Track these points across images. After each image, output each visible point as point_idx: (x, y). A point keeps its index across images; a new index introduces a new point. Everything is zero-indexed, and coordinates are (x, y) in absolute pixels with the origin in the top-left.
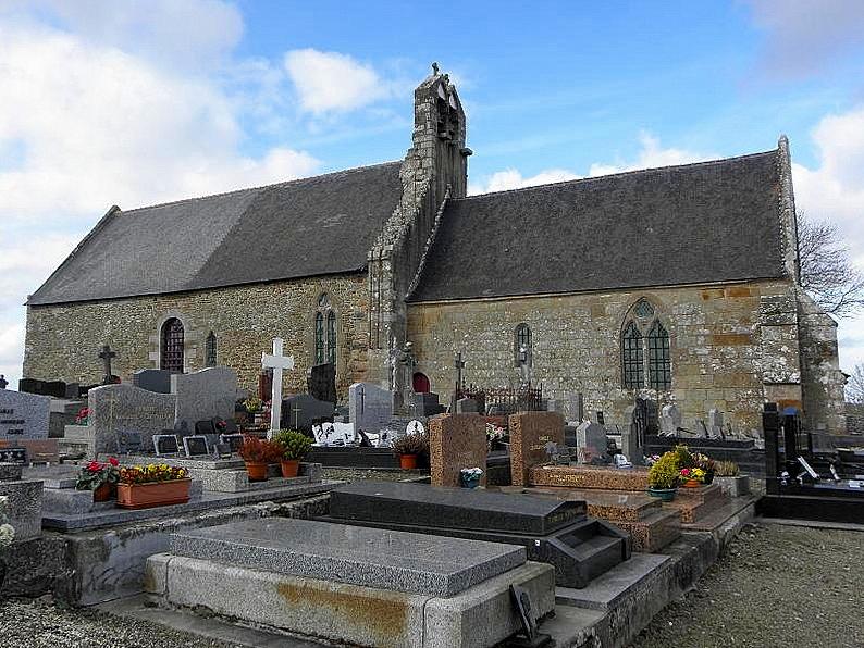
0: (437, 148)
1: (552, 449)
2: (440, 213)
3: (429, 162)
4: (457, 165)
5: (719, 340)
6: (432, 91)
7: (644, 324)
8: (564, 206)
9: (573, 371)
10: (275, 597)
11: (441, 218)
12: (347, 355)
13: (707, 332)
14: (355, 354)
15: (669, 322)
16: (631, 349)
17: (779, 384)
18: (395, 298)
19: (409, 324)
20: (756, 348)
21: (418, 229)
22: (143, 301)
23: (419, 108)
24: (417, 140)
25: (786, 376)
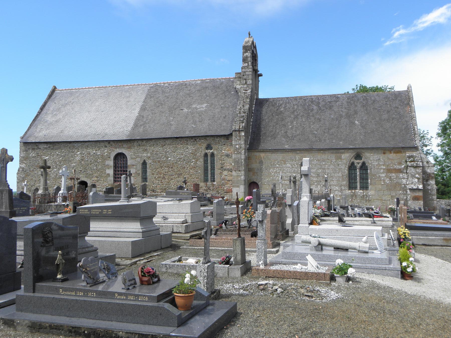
5: (389, 171)
7: (358, 163)
8: (315, 107)
10: (442, 241)
12: (221, 173)
13: (384, 167)
14: (225, 173)
15: (369, 163)
16: (352, 174)
17: (415, 189)
20: (404, 174)
22: (102, 144)
23: (245, 55)
25: (418, 186)
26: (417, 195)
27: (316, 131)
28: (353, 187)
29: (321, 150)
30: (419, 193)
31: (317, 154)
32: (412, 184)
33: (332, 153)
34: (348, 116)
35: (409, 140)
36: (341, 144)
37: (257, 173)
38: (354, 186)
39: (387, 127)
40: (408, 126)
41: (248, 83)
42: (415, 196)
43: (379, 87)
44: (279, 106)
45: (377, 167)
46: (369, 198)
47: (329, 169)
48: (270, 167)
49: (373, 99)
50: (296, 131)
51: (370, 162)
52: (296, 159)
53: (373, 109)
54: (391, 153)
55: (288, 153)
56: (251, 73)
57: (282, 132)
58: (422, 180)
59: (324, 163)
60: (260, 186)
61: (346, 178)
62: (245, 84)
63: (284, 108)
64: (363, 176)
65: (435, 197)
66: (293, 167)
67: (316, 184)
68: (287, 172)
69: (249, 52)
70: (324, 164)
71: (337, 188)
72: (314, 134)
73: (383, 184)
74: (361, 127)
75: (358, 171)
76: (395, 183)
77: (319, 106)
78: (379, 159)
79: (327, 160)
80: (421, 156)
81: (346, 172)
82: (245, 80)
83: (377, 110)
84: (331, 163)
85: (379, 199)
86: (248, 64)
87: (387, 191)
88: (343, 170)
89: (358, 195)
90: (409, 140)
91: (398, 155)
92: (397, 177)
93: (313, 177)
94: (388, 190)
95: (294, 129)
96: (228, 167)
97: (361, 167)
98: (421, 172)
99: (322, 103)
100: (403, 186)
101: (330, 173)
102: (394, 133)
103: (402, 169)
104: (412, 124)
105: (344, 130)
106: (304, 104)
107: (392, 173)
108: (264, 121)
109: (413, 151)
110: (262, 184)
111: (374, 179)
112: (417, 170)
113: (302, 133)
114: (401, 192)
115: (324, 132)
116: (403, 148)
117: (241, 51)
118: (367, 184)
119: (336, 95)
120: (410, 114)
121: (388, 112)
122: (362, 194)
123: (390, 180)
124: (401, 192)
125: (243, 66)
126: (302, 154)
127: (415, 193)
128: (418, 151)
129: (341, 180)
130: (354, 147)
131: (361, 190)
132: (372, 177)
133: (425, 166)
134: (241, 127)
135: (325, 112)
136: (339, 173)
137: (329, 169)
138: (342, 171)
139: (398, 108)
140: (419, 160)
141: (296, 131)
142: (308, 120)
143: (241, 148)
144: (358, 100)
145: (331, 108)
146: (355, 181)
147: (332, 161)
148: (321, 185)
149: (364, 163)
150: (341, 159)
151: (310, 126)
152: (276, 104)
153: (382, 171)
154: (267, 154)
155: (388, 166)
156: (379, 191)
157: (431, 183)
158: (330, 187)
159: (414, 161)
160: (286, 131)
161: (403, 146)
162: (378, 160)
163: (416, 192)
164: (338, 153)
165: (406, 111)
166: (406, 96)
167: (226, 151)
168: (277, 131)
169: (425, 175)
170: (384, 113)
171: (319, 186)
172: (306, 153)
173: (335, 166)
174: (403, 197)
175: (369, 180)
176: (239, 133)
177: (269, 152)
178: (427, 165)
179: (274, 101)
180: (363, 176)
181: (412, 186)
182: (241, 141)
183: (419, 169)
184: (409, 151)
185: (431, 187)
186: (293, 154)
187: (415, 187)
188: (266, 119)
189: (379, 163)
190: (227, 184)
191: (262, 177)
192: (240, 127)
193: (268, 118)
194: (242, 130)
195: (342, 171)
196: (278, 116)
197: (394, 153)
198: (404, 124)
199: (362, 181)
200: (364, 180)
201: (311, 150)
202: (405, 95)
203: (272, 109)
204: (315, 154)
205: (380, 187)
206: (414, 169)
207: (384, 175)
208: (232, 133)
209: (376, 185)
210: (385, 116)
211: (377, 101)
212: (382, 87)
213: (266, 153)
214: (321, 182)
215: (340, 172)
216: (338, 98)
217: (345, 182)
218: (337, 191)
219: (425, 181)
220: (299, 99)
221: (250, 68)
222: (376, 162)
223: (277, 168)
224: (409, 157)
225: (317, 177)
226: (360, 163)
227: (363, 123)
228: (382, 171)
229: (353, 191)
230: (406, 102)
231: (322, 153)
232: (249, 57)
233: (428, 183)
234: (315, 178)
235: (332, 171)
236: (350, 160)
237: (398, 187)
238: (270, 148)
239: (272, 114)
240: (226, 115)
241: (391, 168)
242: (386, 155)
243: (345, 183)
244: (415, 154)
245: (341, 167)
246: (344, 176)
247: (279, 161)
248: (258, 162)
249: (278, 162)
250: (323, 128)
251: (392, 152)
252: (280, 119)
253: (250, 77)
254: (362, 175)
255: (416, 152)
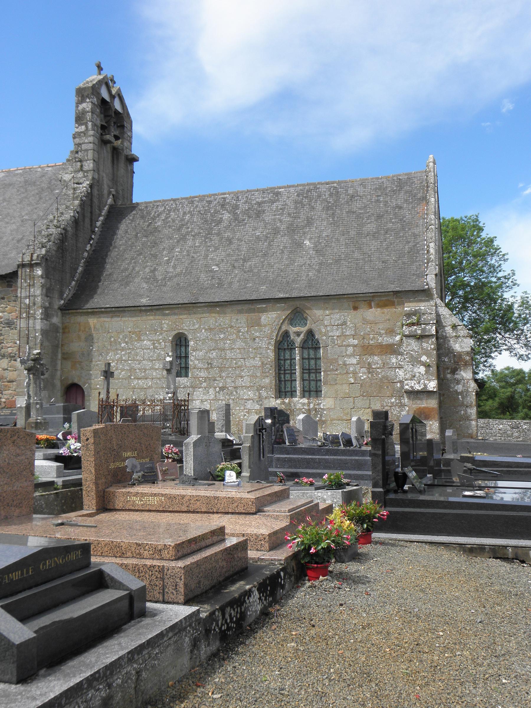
0: (98, 152)
1: (134, 466)
2: (101, 218)
3: (89, 165)
4: (122, 171)
6: (95, 89)
8: (226, 216)
9: (228, 380)
11: (103, 224)
15: (321, 332)
17: (418, 392)
18: (47, 304)
19: (64, 333)
20: (399, 357)
21: (76, 235)
24: (77, 140)
26: (423, 406)
27: (217, 265)
28: (288, 392)
29: (216, 306)
30: (429, 401)
31: (208, 315)
32: (411, 380)
33: (240, 312)
34: (292, 230)
35: (414, 275)
36: (264, 291)
37: (81, 362)
38: (289, 389)
39: (371, 250)
40: (418, 246)
41: (86, 168)
42: (420, 408)
43: (495, 243)
44: (154, 219)
45: (339, 342)
46: (321, 416)
47: (233, 349)
48: (109, 348)
49: (350, 191)
50: (174, 267)
51: (324, 330)
52: (162, 329)
53: (347, 213)
54: (371, 308)
55: (147, 315)
56: (91, 146)
57: (147, 270)
58: (435, 368)
59: (222, 336)
60: (86, 393)
61: (270, 370)
62: (79, 172)
63: (163, 220)
64: (309, 365)
65: (473, 411)
66: (155, 348)
67: (204, 384)
68: (144, 360)
69: (88, 100)
70: (222, 339)
71: (251, 394)
72: (212, 271)
73: (353, 381)
74: (314, 252)
75: (297, 352)
76: (381, 379)
77: (237, 213)
78: (344, 323)
79: (229, 329)
80: (440, 312)
81: (271, 355)
82: (81, 161)
83: (354, 216)
84: (238, 337)
85: (345, 418)
86: (87, 127)
87: (361, 397)
88: (264, 352)
89: (297, 410)
90: (414, 275)
91: (386, 310)
92: (384, 364)
93: (198, 369)
94: (364, 396)
95: (172, 264)
96: (10, 350)
97: (304, 343)
98: (434, 349)
99: (243, 206)
100: (399, 385)
101: (235, 359)
102: (383, 262)
103: (396, 345)
104: (426, 240)
105: (276, 261)
106: (205, 210)
107: (372, 354)
108: (117, 250)
109: (421, 301)
110: (91, 388)
111: (333, 370)
112: (425, 345)
113: (186, 271)
114: (393, 400)
115: (234, 267)
116: (396, 293)
117: (73, 98)
118: (319, 383)
119: (275, 188)
120: (424, 219)
121: (379, 217)
122: (306, 407)
123: (369, 373)
124: (393, 400)
125: (76, 132)
126: (176, 317)
127: (419, 402)
128: (432, 299)
129: (258, 375)
130: (287, 296)
131: (304, 397)
132: (329, 364)
133: (448, 335)
134: (35, 257)
135: (246, 224)
136: (254, 358)
137: (233, 349)
138: (261, 354)
139: (400, 208)
140: (431, 320)
141: (174, 267)
142: (206, 242)
143: (34, 304)
144: (319, 196)
145: (259, 214)
146: (291, 377)
147: (239, 331)
148: (215, 388)
149: (310, 333)
150: (259, 325)
151: (207, 256)
152: (149, 213)
153: (350, 350)
154: (102, 319)
155: (364, 338)
156: (343, 398)
157: (463, 377)
158: (234, 393)
159: (418, 323)
160: (155, 268)
161: (398, 289)
162: (342, 325)
163: (421, 399)
164: (253, 311)
165: (418, 213)
166: (422, 183)
167: (6, 313)
168: (137, 269)
169: (450, 357)
170: (369, 221)
171: (211, 391)
172: (185, 314)
173: (246, 342)
174: (400, 412)
175: (322, 373)
176: (32, 271)
177: (106, 315)
178: (454, 334)
179: (146, 207)
180: (309, 365)
181: (412, 383)
182: (36, 288)
183: (428, 343)
184: (410, 302)
185: (463, 386)
186: (157, 317)
187: (418, 387)
188: (120, 245)
189: (343, 333)
190: (7, 388)
191: (91, 372)
192: (32, 256)
193: (126, 242)
194: (37, 264)
195: (261, 354)
196: (146, 236)
197: (378, 306)
198: (409, 242)
199: (306, 376)
200: (312, 375)
201: (194, 305)
202: (420, 180)
203: (139, 224)
204: (202, 315)
205: (346, 388)
206: (416, 343)
207: (354, 361)
208: (17, 271)
209: (336, 384)
210: (371, 227)
211: (358, 196)
212: (461, 219)
213: (100, 317)
214: (215, 380)
215: (258, 356)
216: (278, 194)
217: (269, 381)
218: (251, 401)
219: (449, 371)
220: (198, 202)
221: (90, 136)
222: (337, 330)
223: (123, 349)
224: (409, 315)
225: (207, 369)
226: (302, 332)
227: (320, 243)
228: (350, 350)
229: (287, 401)
230: (419, 196)
231: (218, 313)
232: (88, 112)
233: (456, 376)
234: (202, 371)
235: (240, 353)
236: (280, 328)
237: (388, 387)
238: (108, 306)
239: (137, 234)
240: (24, 236)
241: (371, 342)
242: (360, 312)
243: (267, 381)
244: (423, 308)
245: (258, 343)
246: (267, 364)
247: (128, 333)
248: (83, 337)
249: (125, 337)
250: (233, 258)
251: (373, 304)
252: (149, 244)
253: (90, 154)
254: (307, 361)
255: (426, 304)
